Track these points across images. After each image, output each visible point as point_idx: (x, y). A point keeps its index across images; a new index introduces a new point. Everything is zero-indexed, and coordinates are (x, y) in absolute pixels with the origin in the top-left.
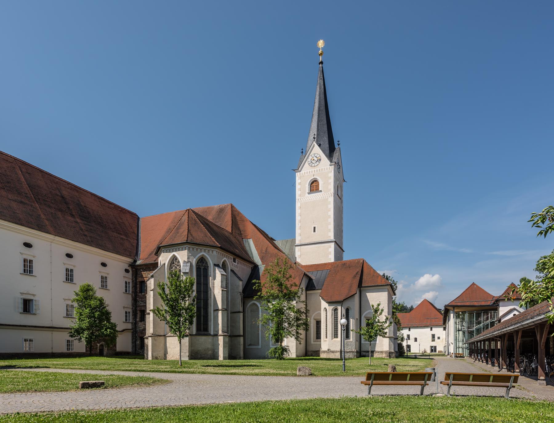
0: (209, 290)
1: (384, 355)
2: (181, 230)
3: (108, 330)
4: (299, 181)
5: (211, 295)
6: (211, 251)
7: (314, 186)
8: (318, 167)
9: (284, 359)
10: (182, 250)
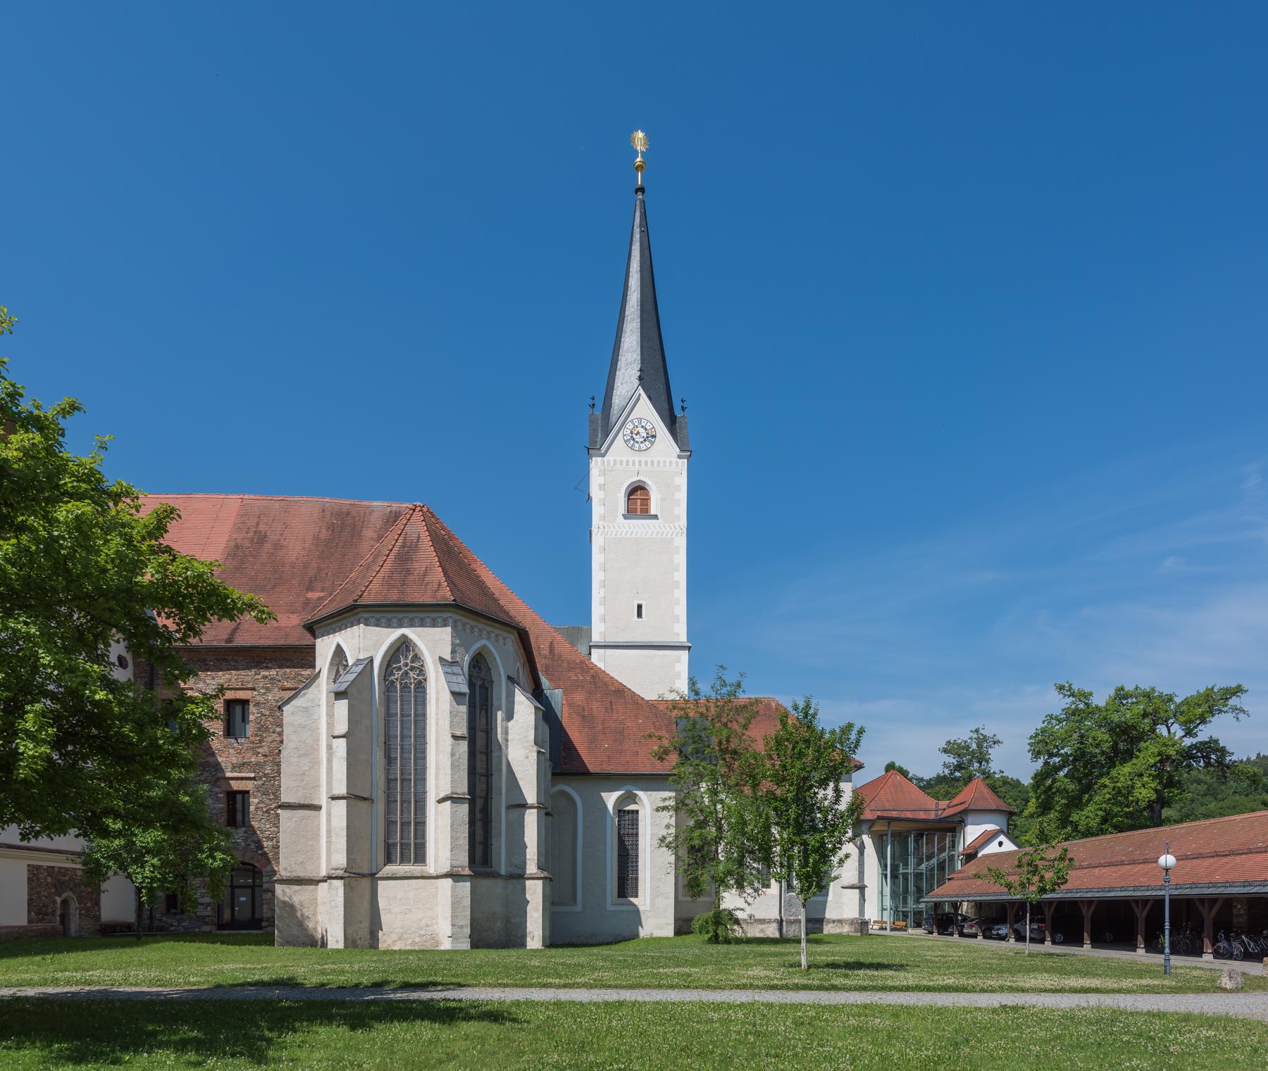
0: (494, 748)
1: (846, 929)
2: (418, 567)
3: (219, 855)
4: (601, 480)
5: (500, 764)
6: (501, 639)
8: (641, 460)
9: (727, 941)
10: (434, 626)
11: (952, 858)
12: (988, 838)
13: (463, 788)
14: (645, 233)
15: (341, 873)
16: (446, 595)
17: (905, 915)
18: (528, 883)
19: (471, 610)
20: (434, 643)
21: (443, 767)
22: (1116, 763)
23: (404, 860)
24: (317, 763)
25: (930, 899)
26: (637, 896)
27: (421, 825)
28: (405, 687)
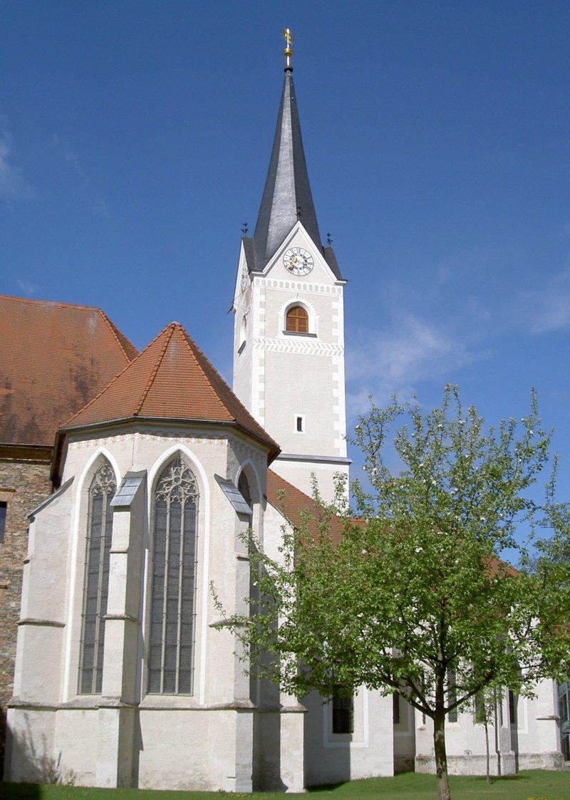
4: (262, 298)
7: (296, 319)
15: (117, 703)
18: (283, 716)
23: (169, 688)
26: (287, 788)
27: (187, 647)
28: (175, 503)
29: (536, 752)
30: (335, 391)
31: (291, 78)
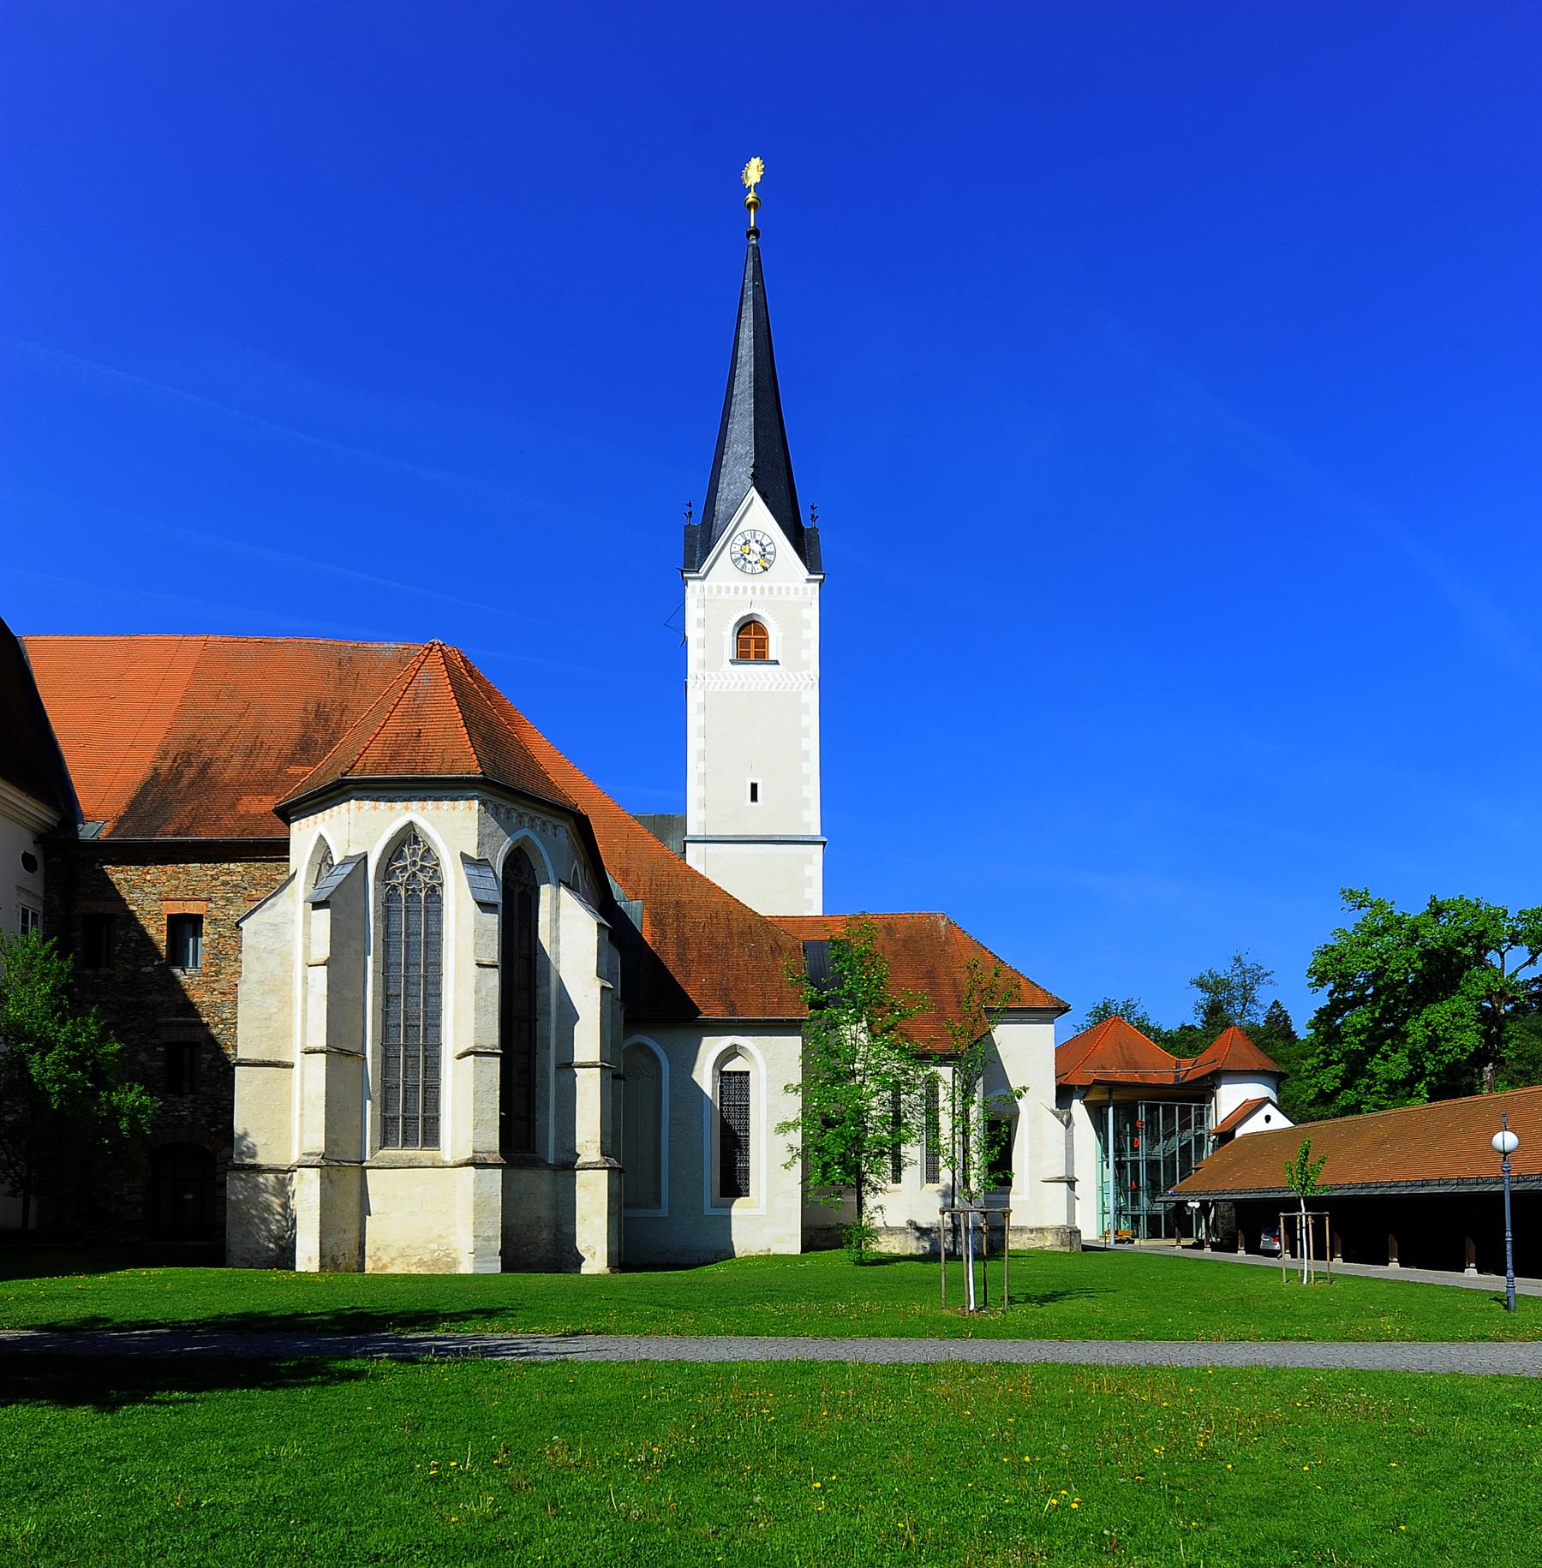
4: (700, 613)
7: (751, 640)
8: (755, 578)
11: (1200, 1140)
12: (1249, 1109)
13: (492, 1038)
14: (760, 290)
15: (316, 1160)
16: (477, 772)
17: (1135, 1220)
19: (505, 787)
20: (454, 829)
21: (467, 1006)
22: (1410, 1008)
24: (287, 1003)
25: (1171, 1195)
28: (412, 895)
29: (1039, 1225)
30: (805, 741)
31: (756, 248)
